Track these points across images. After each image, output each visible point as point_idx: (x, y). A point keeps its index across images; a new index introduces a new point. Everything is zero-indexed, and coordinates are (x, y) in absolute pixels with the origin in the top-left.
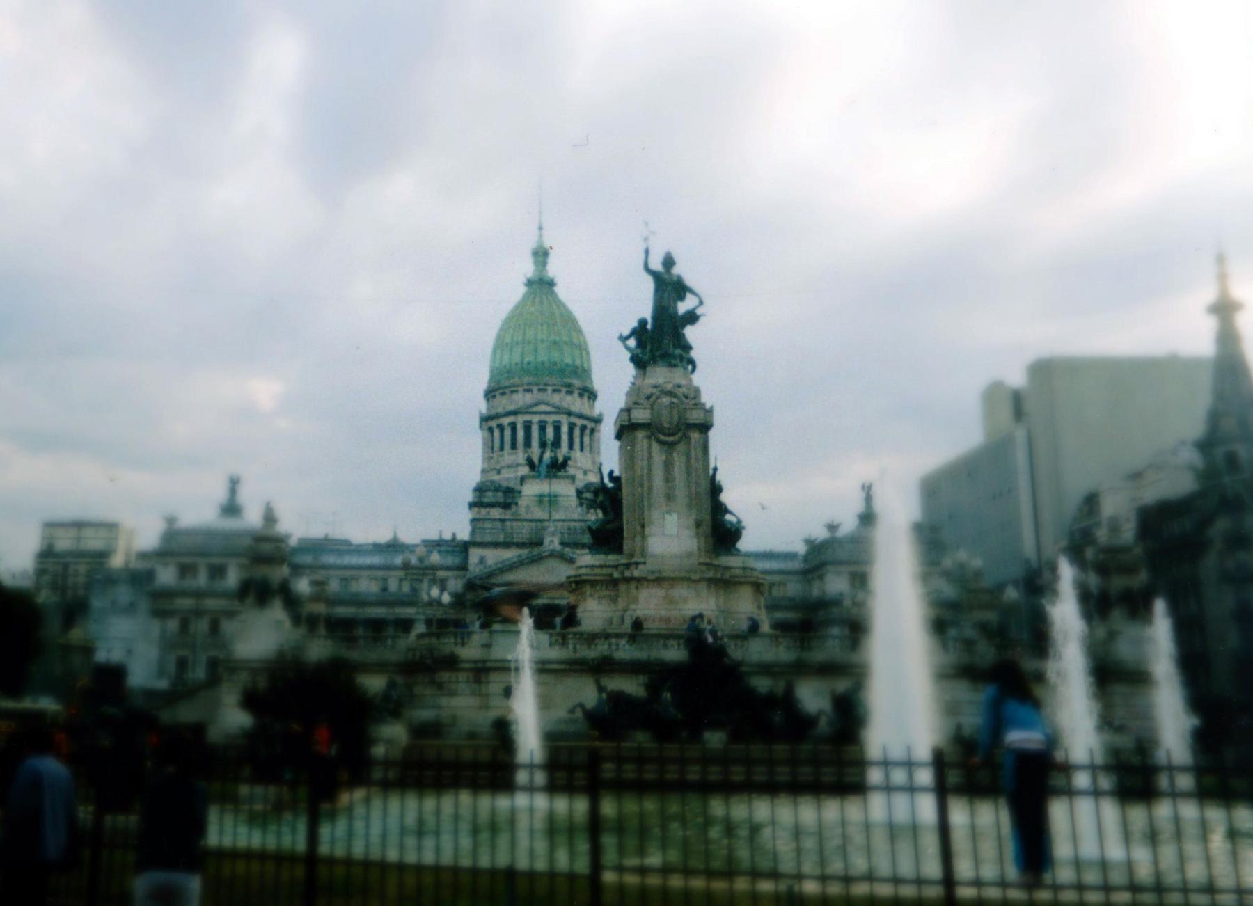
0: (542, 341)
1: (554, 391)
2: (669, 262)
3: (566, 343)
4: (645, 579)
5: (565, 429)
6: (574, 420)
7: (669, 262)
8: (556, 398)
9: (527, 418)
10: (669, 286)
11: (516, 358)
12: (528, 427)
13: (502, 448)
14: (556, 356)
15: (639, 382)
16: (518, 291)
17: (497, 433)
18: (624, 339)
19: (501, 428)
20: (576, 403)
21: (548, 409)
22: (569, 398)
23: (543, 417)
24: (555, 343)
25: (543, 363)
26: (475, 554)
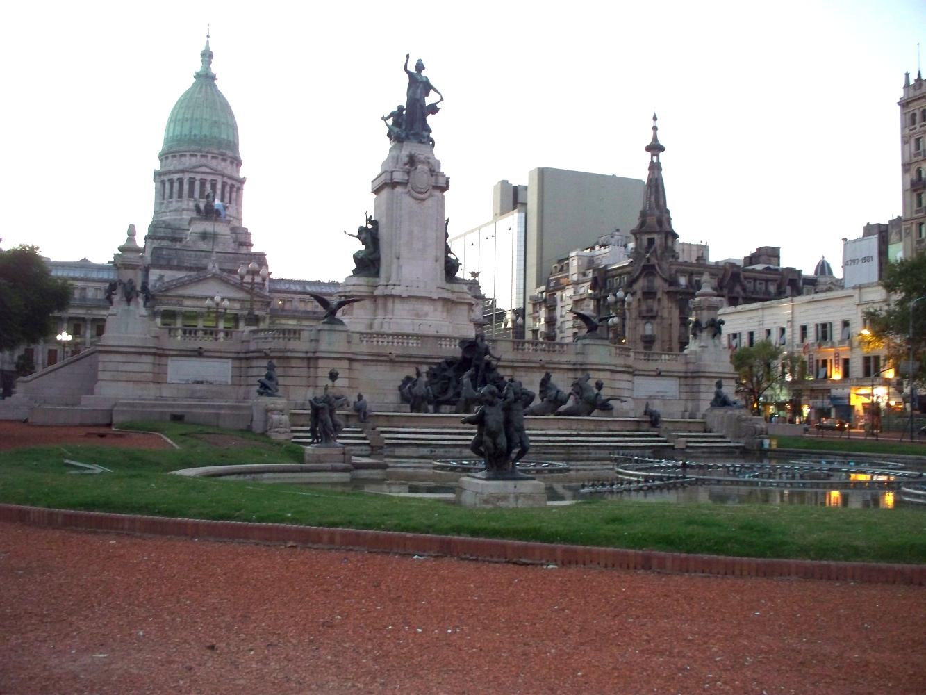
0: (206, 120)
1: (213, 157)
2: (420, 67)
3: (223, 123)
4: (400, 297)
5: (219, 186)
6: (226, 179)
7: (420, 67)
8: (213, 163)
9: (192, 175)
10: (419, 85)
11: (186, 131)
12: (192, 182)
13: (171, 197)
14: (216, 131)
15: (394, 153)
16: (189, 82)
17: (167, 185)
18: (385, 119)
19: (171, 181)
20: (226, 168)
21: (208, 170)
22: (223, 164)
23: (204, 176)
24: (215, 122)
25: (206, 136)
26: (154, 274)
